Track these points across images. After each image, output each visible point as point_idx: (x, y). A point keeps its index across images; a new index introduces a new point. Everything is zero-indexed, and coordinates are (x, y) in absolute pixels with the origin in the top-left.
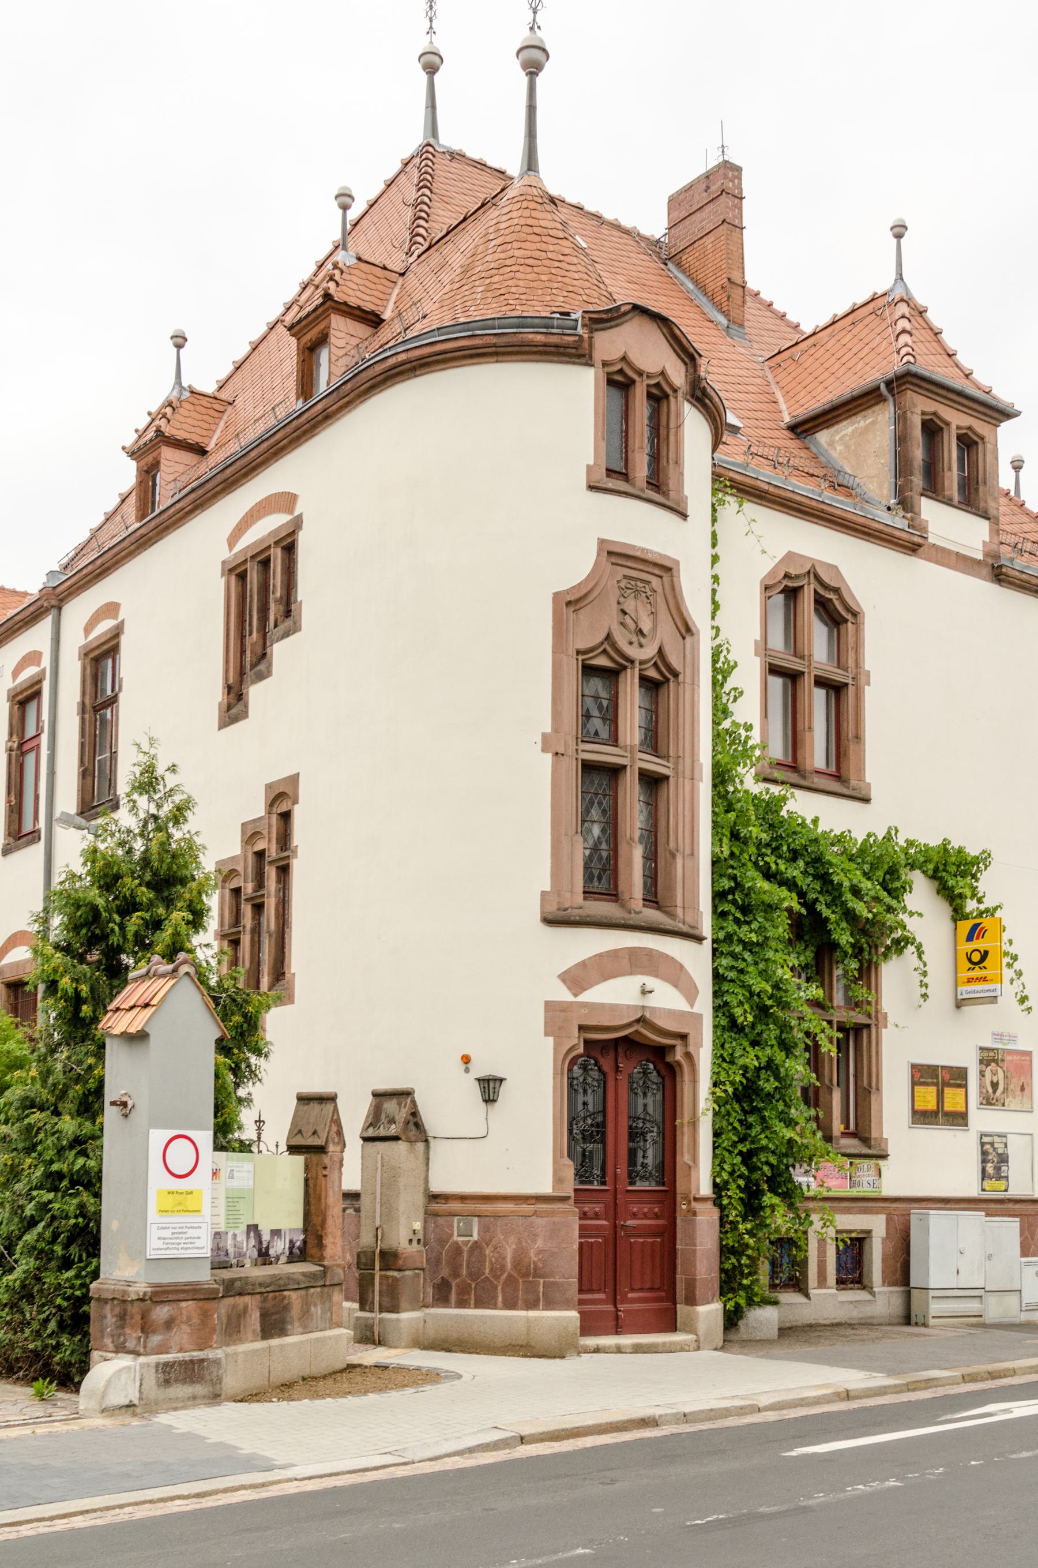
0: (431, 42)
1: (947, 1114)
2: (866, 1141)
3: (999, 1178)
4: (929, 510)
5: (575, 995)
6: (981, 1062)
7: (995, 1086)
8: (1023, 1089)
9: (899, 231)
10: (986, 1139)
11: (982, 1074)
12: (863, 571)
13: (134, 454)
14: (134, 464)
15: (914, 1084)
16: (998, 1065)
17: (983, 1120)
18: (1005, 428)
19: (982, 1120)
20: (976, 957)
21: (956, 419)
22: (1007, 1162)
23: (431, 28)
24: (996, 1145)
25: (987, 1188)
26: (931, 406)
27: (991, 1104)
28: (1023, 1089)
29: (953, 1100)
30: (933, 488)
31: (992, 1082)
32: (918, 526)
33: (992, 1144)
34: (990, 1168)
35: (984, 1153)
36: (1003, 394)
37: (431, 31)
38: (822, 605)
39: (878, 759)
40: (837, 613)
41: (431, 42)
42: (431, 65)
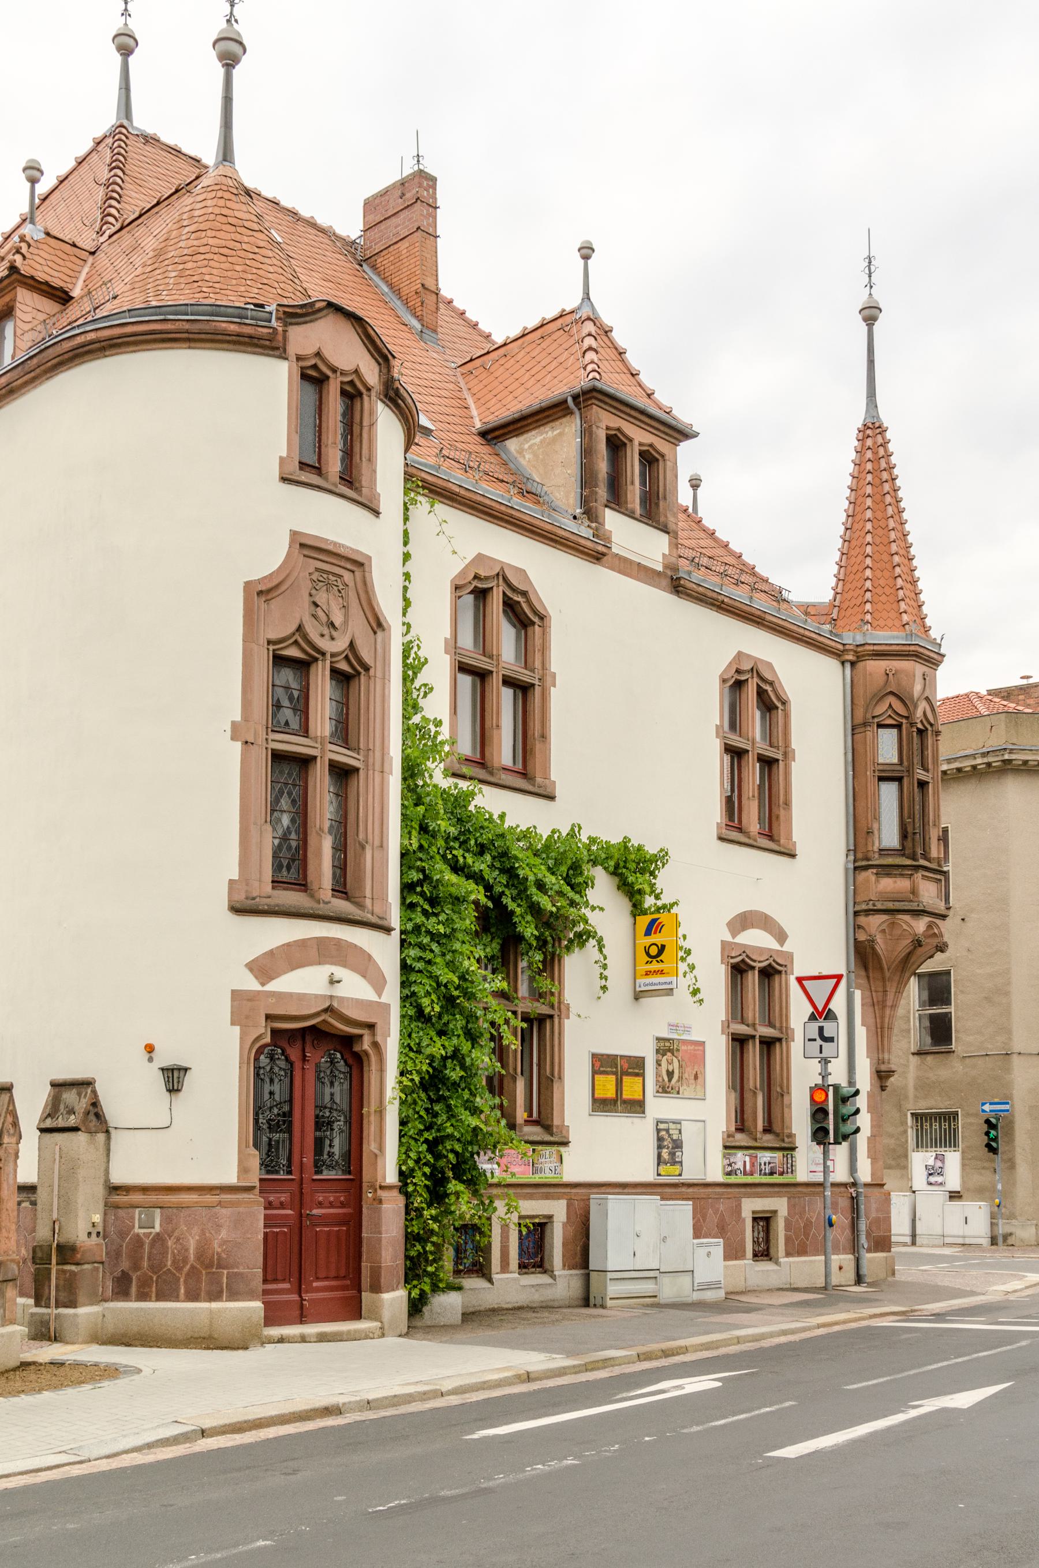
0: (126, 24)
1: (625, 1102)
2: (548, 1128)
3: (674, 1163)
4: (612, 520)
5: (263, 984)
6: (658, 1051)
7: (670, 1074)
8: (696, 1077)
9: (586, 252)
10: (661, 1126)
11: (658, 1063)
12: (549, 575)
15: (595, 1072)
17: (658, 1107)
18: (684, 448)
19: (658, 1107)
20: (654, 951)
21: (639, 436)
23: (126, 10)
24: (671, 1132)
26: (615, 422)
27: (666, 1092)
28: (696, 1077)
29: (631, 1088)
30: (617, 499)
31: (668, 1071)
32: (600, 533)
33: (667, 1131)
34: (665, 1154)
35: (660, 1139)
36: (683, 415)
37: (126, 13)
38: (511, 607)
39: (564, 756)
40: (524, 615)
41: (126, 24)
42: (870, 315)
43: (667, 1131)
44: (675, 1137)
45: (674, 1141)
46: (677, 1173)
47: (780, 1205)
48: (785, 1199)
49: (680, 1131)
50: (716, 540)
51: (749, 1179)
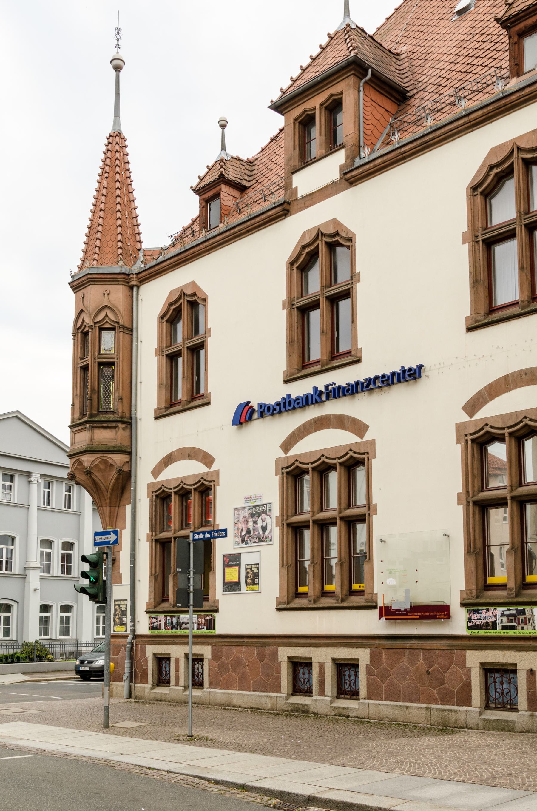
0: (118, 52)
5: (471, 417)
13: (198, 191)
14: (198, 197)
16: (266, 514)
22: (258, 576)
23: (118, 44)
24: (253, 569)
25: (116, 630)
27: (262, 541)
31: (262, 527)
33: (251, 569)
37: (118, 46)
41: (118, 52)
43: (251, 569)
44: (123, 609)
45: (122, 611)
46: (124, 630)
47: (206, 651)
48: (368, 651)
49: (258, 568)
50: (83, 264)
51: (174, 632)
